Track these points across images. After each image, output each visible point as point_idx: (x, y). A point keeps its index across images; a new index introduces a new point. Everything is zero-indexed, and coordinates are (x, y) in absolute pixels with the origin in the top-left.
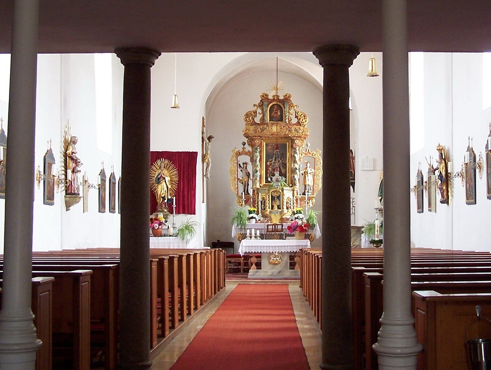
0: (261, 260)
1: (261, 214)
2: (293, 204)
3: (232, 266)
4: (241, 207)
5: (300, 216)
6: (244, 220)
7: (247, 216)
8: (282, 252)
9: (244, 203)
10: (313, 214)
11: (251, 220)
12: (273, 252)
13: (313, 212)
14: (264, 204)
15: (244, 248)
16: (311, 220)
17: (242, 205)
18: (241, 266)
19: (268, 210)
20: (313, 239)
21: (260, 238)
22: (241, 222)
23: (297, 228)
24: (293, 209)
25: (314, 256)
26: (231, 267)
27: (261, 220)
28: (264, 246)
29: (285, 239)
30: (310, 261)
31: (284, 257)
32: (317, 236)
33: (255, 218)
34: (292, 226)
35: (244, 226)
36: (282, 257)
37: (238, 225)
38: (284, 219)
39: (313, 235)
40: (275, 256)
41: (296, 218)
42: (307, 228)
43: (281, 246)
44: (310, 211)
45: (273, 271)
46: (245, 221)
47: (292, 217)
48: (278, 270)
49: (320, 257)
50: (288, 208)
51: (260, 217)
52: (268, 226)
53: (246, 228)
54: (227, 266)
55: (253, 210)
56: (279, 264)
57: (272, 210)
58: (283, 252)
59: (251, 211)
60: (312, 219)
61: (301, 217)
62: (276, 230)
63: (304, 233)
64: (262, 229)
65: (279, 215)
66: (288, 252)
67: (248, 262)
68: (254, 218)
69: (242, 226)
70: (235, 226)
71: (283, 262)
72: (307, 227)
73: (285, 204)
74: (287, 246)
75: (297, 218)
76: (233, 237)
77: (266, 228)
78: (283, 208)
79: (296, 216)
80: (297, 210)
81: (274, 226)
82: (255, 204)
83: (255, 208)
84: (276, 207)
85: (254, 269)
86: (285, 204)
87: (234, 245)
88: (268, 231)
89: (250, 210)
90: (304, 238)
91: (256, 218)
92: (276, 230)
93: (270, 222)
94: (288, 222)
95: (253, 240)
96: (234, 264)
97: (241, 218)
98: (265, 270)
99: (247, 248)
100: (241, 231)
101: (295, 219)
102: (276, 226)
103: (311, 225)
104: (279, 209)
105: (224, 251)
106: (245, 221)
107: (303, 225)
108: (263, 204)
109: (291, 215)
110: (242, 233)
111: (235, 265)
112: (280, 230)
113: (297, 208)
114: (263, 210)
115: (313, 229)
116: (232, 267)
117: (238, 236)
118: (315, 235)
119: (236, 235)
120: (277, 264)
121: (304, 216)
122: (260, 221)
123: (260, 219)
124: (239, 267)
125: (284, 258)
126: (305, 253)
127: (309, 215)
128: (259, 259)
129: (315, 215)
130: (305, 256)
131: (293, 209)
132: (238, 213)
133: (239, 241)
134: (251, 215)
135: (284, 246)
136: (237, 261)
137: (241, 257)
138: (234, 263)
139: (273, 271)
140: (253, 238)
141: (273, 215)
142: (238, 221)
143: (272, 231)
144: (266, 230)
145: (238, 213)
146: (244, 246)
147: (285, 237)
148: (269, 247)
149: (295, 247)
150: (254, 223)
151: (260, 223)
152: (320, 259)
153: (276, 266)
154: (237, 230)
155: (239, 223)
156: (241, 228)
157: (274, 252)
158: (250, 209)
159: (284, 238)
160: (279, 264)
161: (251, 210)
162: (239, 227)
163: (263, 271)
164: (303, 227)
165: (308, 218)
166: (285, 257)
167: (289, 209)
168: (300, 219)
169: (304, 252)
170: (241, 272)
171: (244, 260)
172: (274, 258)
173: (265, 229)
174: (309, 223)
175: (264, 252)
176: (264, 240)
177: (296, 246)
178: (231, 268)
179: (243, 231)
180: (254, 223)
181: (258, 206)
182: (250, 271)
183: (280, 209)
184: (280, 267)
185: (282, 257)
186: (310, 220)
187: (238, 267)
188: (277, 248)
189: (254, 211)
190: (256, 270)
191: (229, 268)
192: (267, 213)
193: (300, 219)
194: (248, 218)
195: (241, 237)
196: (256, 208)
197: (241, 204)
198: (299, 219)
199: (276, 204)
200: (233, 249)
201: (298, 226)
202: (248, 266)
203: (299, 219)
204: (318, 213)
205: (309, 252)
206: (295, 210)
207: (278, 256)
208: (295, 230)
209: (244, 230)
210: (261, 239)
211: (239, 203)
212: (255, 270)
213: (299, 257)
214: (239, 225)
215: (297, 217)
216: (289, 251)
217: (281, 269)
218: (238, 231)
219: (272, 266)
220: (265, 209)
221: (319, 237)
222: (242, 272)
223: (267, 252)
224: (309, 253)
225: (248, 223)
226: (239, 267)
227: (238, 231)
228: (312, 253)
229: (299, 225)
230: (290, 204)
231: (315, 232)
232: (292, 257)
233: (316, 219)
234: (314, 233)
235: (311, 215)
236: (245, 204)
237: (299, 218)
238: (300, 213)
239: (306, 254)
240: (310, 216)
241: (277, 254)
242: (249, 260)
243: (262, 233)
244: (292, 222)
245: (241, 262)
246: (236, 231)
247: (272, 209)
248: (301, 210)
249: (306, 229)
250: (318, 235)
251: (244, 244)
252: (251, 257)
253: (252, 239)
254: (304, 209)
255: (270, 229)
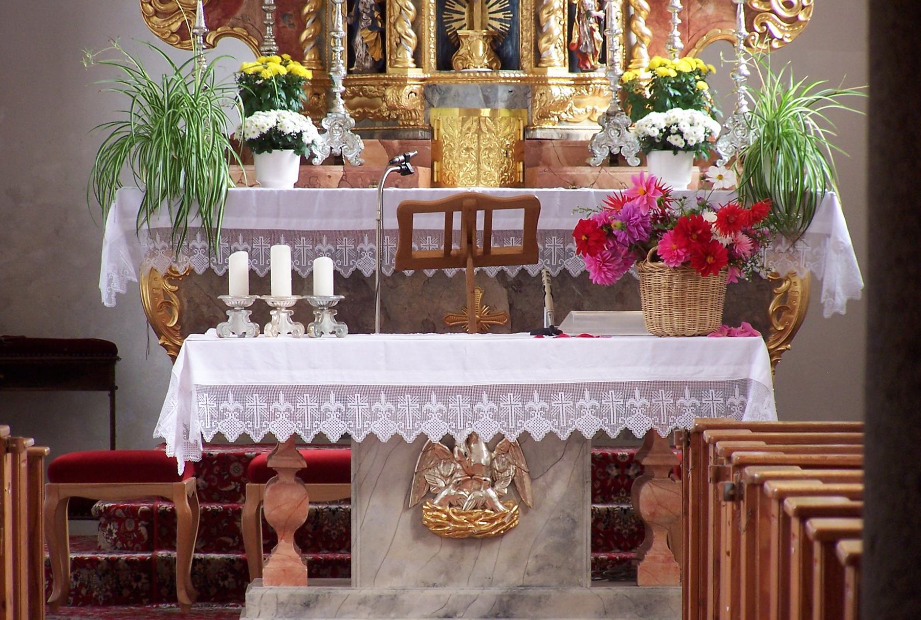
0: (348, 501)
1: (348, 106)
2: (628, 21)
3: (99, 550)
4: (179, 55)
5: (686, 129)
6: (200, 162)
7: (229, 129)
8: (526, 435)
9: (200, 21)
10: (797, 110)
11: (265, 160)
12: (449, 441)
13: (797, 94)
14: (372, 28)
15: (202, 406)
16: (781, 158)
17: (183, 33)
18: (173, 548)
19: (414, 73)
20: (794, 317)
21: (338, 319)
22: (175, 180)
23: (655, 235)
24: (626, 68)
25: (804, 529)
26: (87, 556)
27: (350, 156)
28: (371, 392)
29: (554, 331)
30: (766, 553)
31: (541, 482)
32: (832, 294)
33: (294, 142)
34: (617, 224)
35: (206, 216)
36: (526, 480)
37: (148, 206)
38: (550, 145)
39: (798, 288)
40: (472, 474)
41: (650, 144)
42: (744, 239)
43: (524, 392)
44: (771, 87)
45: (451, 592)
46: (213, 163)
47: (614, 133)
48: (496, 591)
49: (854, 560)
50: (585, 57)
51: (337, 136)
52: (406, 213)
53: (227, 222)
54: (58, 549)
55: (283, 71)
56: (499, 536)
57: (444, 74)
58: (538, 436)
59: (266, 86)
60: (789, 154)
61: (695, 135)
62: (479, 245)
63: (717, 282)
64: (357, 236)
65: (503, 113)
66: (576, 436)
67: (239, 512)
68: (287, 147)
69: (182, 213)
70: (123, 214)
71: (540, 521)
72: (745, 233)
73: (556, 25)
74: (575, 390)
75: (665, 145)
76: (107, 300)
77: (392, 223)
78: (538, 58)
79: (654, 123)
80: (662, 72)
81: (457, 218)
82: (303, 28)
83: (299, 57)
84: (481, 48)
85: (286, 576)
86: (556, 25)
87: (119, 367)
88: (405, 256)
89: (257, 75)
90: (715, 317)
91: (306, 139)
92: (479, 245)
93: (423, 173)
94: (586, 170)
95: (284, 338)
96: (113, 527)
97: (179, 142)
98: (385, 587)
99: (231, 405)
100: (176, 250)
101: (643, 156)
102: (480, 215)
103: (781, 201)
104: (504, 67)
105: (31, 441)
106: (213, 163)
107: (710, 217)
108: (365, 18)
109: (608, 115)
110: (181, 270)
111: (125, 541)
112: (515, 245)
113: (657, 60)
114: (364, 71)
115: (794, 235)
116: (101, 556)
117: (153, 296)
118: (816, 283)
119: (130, 282)
120: (482, 539)
121: (716, 128)
122: (338, 170)
123: (337, 151)
124: (162, 553)
125: (549, 486)
126: (726, 485)
127: (767, 114)
128: (329, 491)
129: (813, 117)
130: (727, 509)
131: (626, 68)
132: (155, 102)
133: (159, 335)
134: (264, 121)
135: (548, 391)
136: (144, 507)
137: (180, 479)
138: (120, 521)
139: (451, 592)
140: (281, 318)
141: (455, 112)
142: (150, 170)
143: (448, 259)
144: (392, 246)
145: (155, 102)
146: (202, 389)
147: (559, 317)
148: (420, 393)
149: (638, 401)
150: (290, 187)
151: (343, 182)
152: (850, 575)
153: (471, 552)
154: (145, 244)
155: (160, 184)
156: (179, 232)
157: (460, 439)
158: (251, 65)
159: (547, 322)
160: (508, 539)
161: (267, 74)
162: (163, 219)
163: (363, 602)
164: (707, 226)
165: (752, 138)
166: (553, 482)
167: (593, 62)
168: (687, 148)
169: (719, 476)
170: (173, 598)
171: (204, 494)
172: (459, 486)
173: (383, 232)
174: (762, 180)
175: (372, 437)
176: (377, 338)
177: (650, 388)
178: (93, 561)
179: (191, 252)
180: (290, 187)
181: (321, 42)
182: (253, 592)
183: (517, 66)
184: (514, 561)
185: (526, 480)
186: (774, 162)
187: (148, 555)
188: (485, 405)
189: (290, 83)
190: (304, 590)
191: (77, 563)
192: (405, 102)
193: (687, 148)
194: (233, 142)
195: (175, 301)
196: (309, 56)
197: (175, 27)
198: (676, 149)
199: (477, 24)
200: (106, 394)
201: (665, 218)
202: (240, 547)
203: (676, 149)
204: (842, 100)
205: (756, 472)
206: (642, 74)
207: (490, 467)
208: (639, 251)
209: (199, 243)
210: (345, 327)
211: (156, 13)
212: (292, 589)
213: (677, 472)
214: (163, 206)
215: (655, 133)
216: (589, 434)
217: (514, 578)
218: (153, 253)
219: (445, 551)
220: (380, 66)
221: (850, 303)
222: (182, 595)
223: (397, 439)
224: (758, 484)
225: (235, 189)
226: (162, 553)
227: (153, 253)
228: (782, 496)
229: (674, 210)
230: (602, 24)
231: (818, 258)
232: (614, 472)
233: (820, 149)
234: (803, 271)
235: (777, 116)
236: (211, 27)
237: (673, 140)
238: (690, 100)
239: (734, 496)
240: (770, 126)
241: (485, 458)
242: (237, 495)
243: (360, 264)
244: (618, 172)
245: (178, 512)
246: (134, 255)
247: (445, 63)
248: (699, 72)
249: (730, 247)
250: (839, 289)
251: (202, 376)
252: (263, 474)
253: (268, 327)
254: (717, 64)
255: (425, 233)
